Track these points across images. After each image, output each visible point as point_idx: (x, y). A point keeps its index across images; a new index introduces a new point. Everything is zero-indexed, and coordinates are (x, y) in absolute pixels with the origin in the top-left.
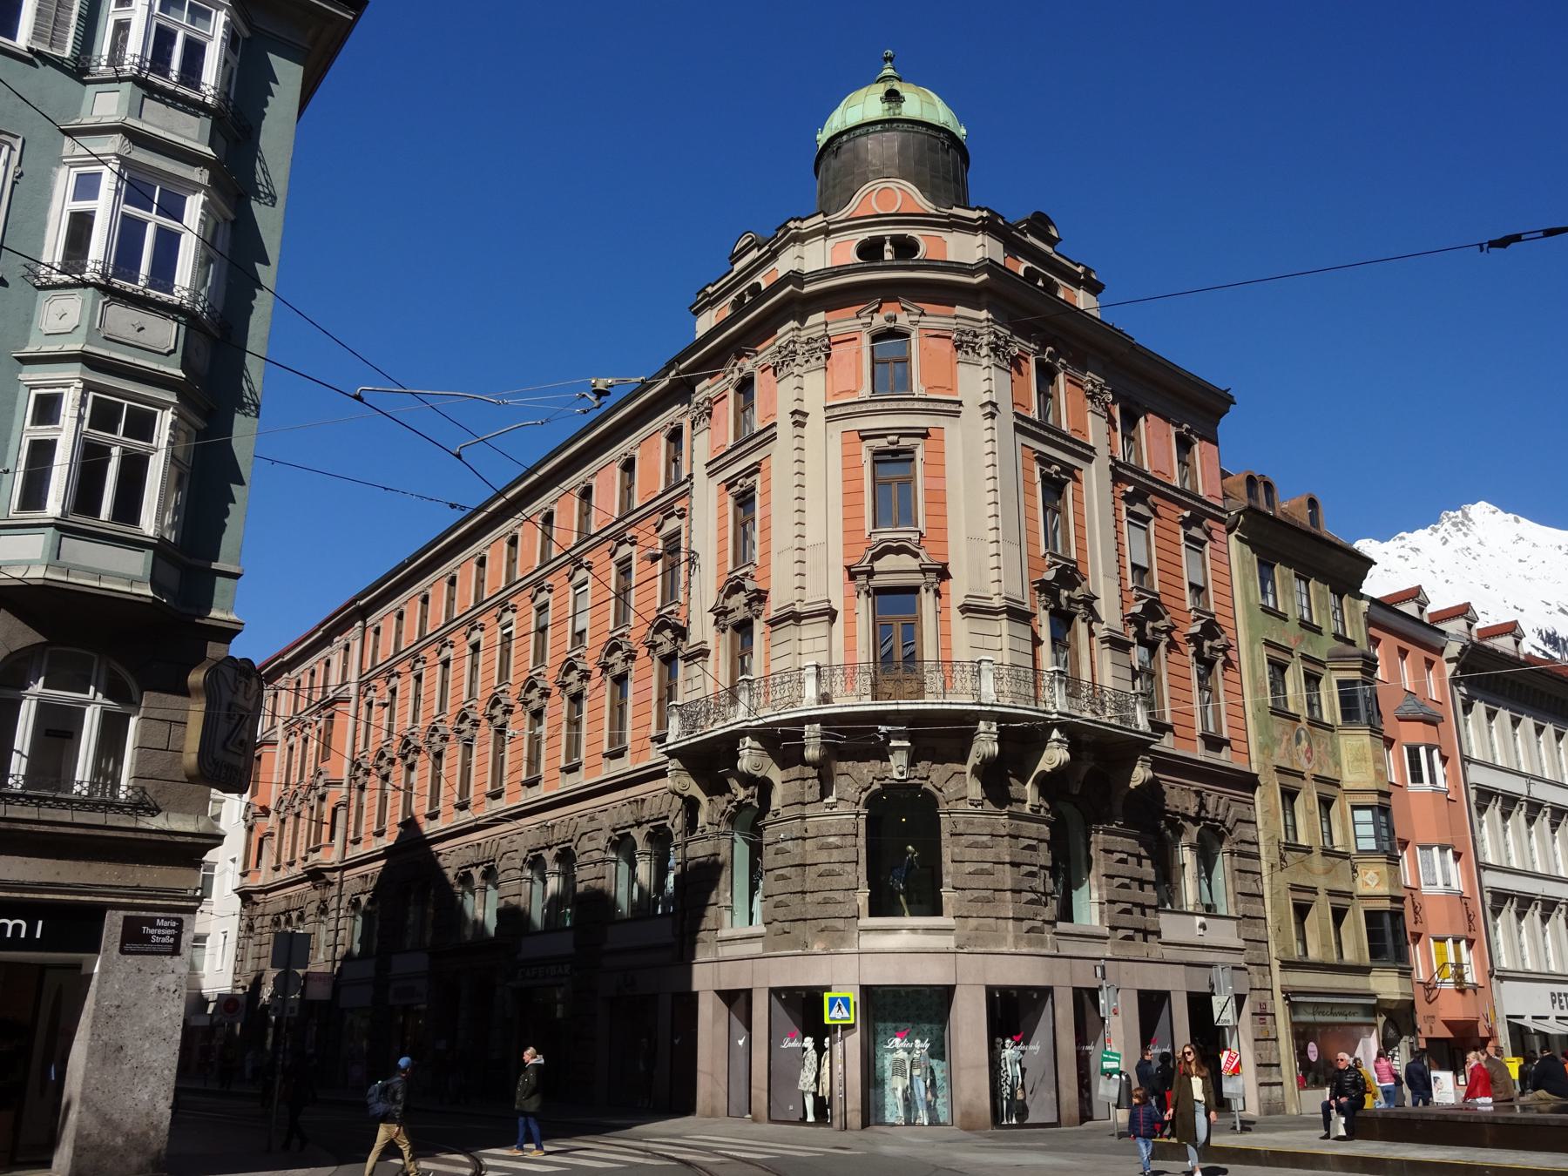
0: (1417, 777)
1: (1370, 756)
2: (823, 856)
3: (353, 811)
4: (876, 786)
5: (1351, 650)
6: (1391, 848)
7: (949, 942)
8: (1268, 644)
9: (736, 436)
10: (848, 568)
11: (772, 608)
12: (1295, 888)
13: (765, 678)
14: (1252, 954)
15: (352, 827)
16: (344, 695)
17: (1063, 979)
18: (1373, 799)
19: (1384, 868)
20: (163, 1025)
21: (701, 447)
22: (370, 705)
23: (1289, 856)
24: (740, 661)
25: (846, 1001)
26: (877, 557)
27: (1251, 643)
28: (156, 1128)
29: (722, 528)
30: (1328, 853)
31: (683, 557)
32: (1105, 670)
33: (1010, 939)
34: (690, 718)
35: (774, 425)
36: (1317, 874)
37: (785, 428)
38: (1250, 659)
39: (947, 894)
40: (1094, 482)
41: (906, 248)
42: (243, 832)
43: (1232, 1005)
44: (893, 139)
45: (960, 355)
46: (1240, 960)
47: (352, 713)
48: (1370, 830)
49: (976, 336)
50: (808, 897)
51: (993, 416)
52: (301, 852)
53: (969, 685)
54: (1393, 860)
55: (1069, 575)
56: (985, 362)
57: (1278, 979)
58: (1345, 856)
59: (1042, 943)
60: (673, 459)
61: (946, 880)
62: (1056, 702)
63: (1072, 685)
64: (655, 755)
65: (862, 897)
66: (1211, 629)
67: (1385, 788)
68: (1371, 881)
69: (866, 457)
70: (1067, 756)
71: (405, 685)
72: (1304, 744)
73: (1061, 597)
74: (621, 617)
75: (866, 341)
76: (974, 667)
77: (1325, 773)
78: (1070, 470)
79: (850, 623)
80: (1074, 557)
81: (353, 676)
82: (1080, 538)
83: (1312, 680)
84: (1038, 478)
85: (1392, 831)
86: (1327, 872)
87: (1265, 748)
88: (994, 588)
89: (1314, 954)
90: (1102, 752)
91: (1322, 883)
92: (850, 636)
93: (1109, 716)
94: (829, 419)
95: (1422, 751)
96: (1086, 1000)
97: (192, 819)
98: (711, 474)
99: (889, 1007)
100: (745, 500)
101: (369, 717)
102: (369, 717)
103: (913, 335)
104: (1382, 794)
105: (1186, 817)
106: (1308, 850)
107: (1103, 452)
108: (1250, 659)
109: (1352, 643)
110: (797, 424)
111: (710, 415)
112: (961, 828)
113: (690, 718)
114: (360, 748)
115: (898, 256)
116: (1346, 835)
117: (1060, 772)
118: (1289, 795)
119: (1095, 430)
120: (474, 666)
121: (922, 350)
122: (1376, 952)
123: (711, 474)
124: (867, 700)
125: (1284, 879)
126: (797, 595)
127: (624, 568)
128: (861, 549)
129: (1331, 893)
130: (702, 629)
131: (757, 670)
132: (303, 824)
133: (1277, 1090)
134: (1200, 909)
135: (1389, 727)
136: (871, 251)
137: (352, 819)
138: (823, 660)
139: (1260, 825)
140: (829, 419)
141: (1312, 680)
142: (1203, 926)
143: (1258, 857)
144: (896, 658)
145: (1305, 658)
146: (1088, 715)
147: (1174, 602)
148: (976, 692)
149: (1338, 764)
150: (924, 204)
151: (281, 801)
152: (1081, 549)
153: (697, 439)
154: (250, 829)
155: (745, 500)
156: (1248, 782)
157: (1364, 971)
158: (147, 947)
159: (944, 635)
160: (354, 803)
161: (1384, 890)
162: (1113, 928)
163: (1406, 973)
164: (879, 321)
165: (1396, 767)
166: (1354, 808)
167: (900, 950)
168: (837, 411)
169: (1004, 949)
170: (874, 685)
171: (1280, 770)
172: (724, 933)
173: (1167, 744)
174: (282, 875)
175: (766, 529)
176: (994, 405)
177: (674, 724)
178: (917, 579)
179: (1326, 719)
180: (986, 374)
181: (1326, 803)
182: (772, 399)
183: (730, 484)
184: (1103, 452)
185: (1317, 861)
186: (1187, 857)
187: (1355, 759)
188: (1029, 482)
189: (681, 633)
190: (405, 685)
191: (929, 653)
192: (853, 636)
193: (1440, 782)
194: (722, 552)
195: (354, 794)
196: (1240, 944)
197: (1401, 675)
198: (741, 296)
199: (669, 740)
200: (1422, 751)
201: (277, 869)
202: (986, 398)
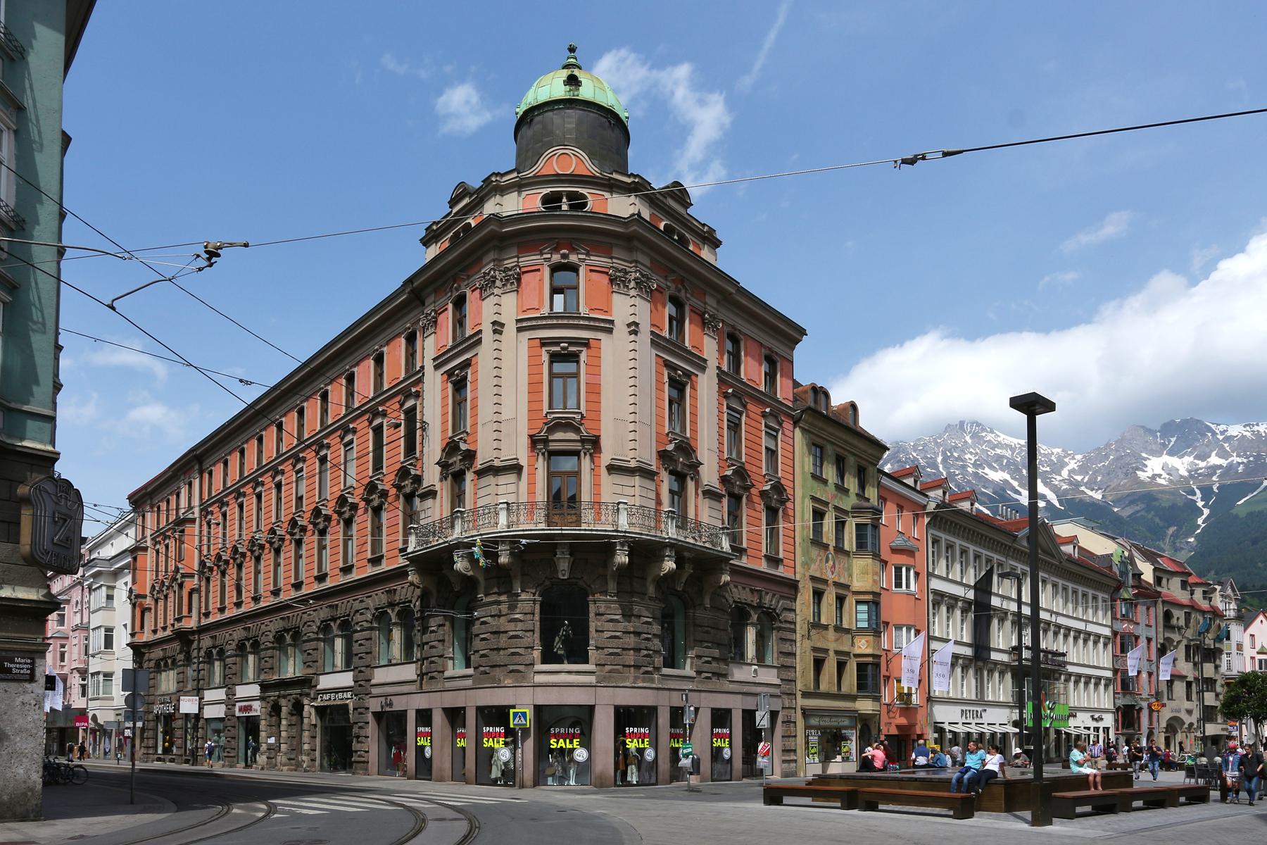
0: (899, 585)
1: (870, 571)
2: (511, 626)
3: (203, 594)
4: (547, 583)
5: (866, 504)
6: (876, 628)
7: (591, 679)
8: (814, 499)
9: (454, 339)
10: (531, 436)
11: (479, 463)
12: (815, 649)
13: (475, 511)
14: (786, 688)
15: (203, 605)
16: (191, 516)
17: (665, 703)
18: (869, 597)
19: (871, 638)
20: (29, 726)
21: (429, 347)
22: (209, 524)
23: (813, 632)
24: (458, 498)
25: (524, 714)
26: (551, 430)
27: (803, 497)
28: (32, 790)
29: (444, 406)
30: (838, 629)
31: (418, 425)
32: (707, 514)
33: (632, 679)
34: (424, 534)
35: (480, 331)
36: (831, 642)
37: (487, 335)
38: (802, 509)
39: (592, 653)
40: (706, 388)
41: (578, 203)
42: (129, 607)
43: (767, 716)
44: (573, 115)
45: (615, 288)
46: (777, 691)
47: (197, 533)
48: (865, 616)
49: (626, 273)
50: (502, 652)
51: (635, 333)
52: (170, 620)
53: (610, 518)
54: (877, 634)
55: (686, 448)
56: (633, 292)
57: (801, 702)
58: (848, 631)
59: (652, 681)
60: (411, 355)
61: (591, 642)
62: (671, 532)
63: (682, 522)
64: (402, 562)
65: (537, 654)
66: (778, 488)
67: (878, 590)
68: (863, 646)
69: (545, 358)
70: (674, 566)
71: (233, 511)
72: (831, 563)
73: (679, 461)
74: (378, 466)
75: (546, 272)
76: (618, 508)
77: (842, 581)
78: (688, 375)
79: (532, 474)
80: (688, 435)
81: (196, 502)
82: (694, 423)
83: (840, 525)
84: (666, 379)
85: (878, 615)
86: (837, 640)
87: (806, 565)
88: (632, 454)
89: (824, 687)
90: (700, 565)
91: (832, 646)
92: (532, 484)
93: (703, 543)
94: (519, 330)
95: (904, 570)
96: (677, 714)
97: (34, 590)
98: (437, 367)
99: (547, 718)
100: (459, 385)
101: (209, 533)
102: (209, 533)
103: (582, 271)
104: (874, 593)
105: (753, 607)
106: (826, 627)
107: (712, 364)
108: (802, 509)
109: (868, 500)
110: (495, 332)
111: (436, 322)
112: (602, 610)
113: (424, 534)
114: (205, 552)
115: (571, 207)
116: (850, 619)
117: (671, 575)
118: (818, 595)
119: (710, 348)
120: (279, 499)
121: (588, 281)
122: (861, 686)
123: (437, 367)
124: (542, 526)
125: (808, 644)
126: (496, 453)
127: (378, 431)
128: (540, 424)
129: (837, 652)
130: (432, 476)
131: (469, 504)
132: (170, 600)
133: (793, 765)
134: (755, 661)
135: (885, 553)
136: (551, 201)
137: (203, 599)
138: (511, 499)
139: (798, 611)
140: (519, 330)
141: (840, 525)
142: (755, 671)
143: (794, 631)
144: (562, 501)
145: (836, 508)
146: (692, 541)
147: (754, 469)
148: (615, 523)
149: (850, 575)
150: (588, 167)
151: (153, 587)
152: (694, 431)
153: (427, 341)
154: (134, 605)
155: (459, 385)
156: (793, 586)
157: (853, 698)
158: (10, 677)
159: (597, 485)
160: (203, 589)
161: (869, 651)
162: (699, 673)
163: (877, 699)
164: (556, 258)
165: (887, 579)
166: (858, 602)
167: (563, 684)
168: (524, 324)
169: (628, 684)
170: (547, 516)
171: (813, 578)
172: (447, 674)
173: (744, 562)
174: (160, 634)
175: (474, 407)
176: (636, 324)
177: (412, 540)
178: (578, 446)
179: (847, 547)
180: (633, 301)
181: (841, 600)
182: (479, 313)
183: (450, 373)
184: (712, 364)
185: (831, 634)
186: (751, 634)
187: (861, 573)
188: (659, 382)
189: (418, 480)
190: (233, 511)
191: (586, 496)
192: (534, 484)
193: (913, 587)
194: (444, 422)
195: (203, 583)
196: (778, 682)
197: (896, 525)
198: (457, 234)
199: (409, 550)
200: (904, 570)
201: (155, 632)
202: (631, 319)
